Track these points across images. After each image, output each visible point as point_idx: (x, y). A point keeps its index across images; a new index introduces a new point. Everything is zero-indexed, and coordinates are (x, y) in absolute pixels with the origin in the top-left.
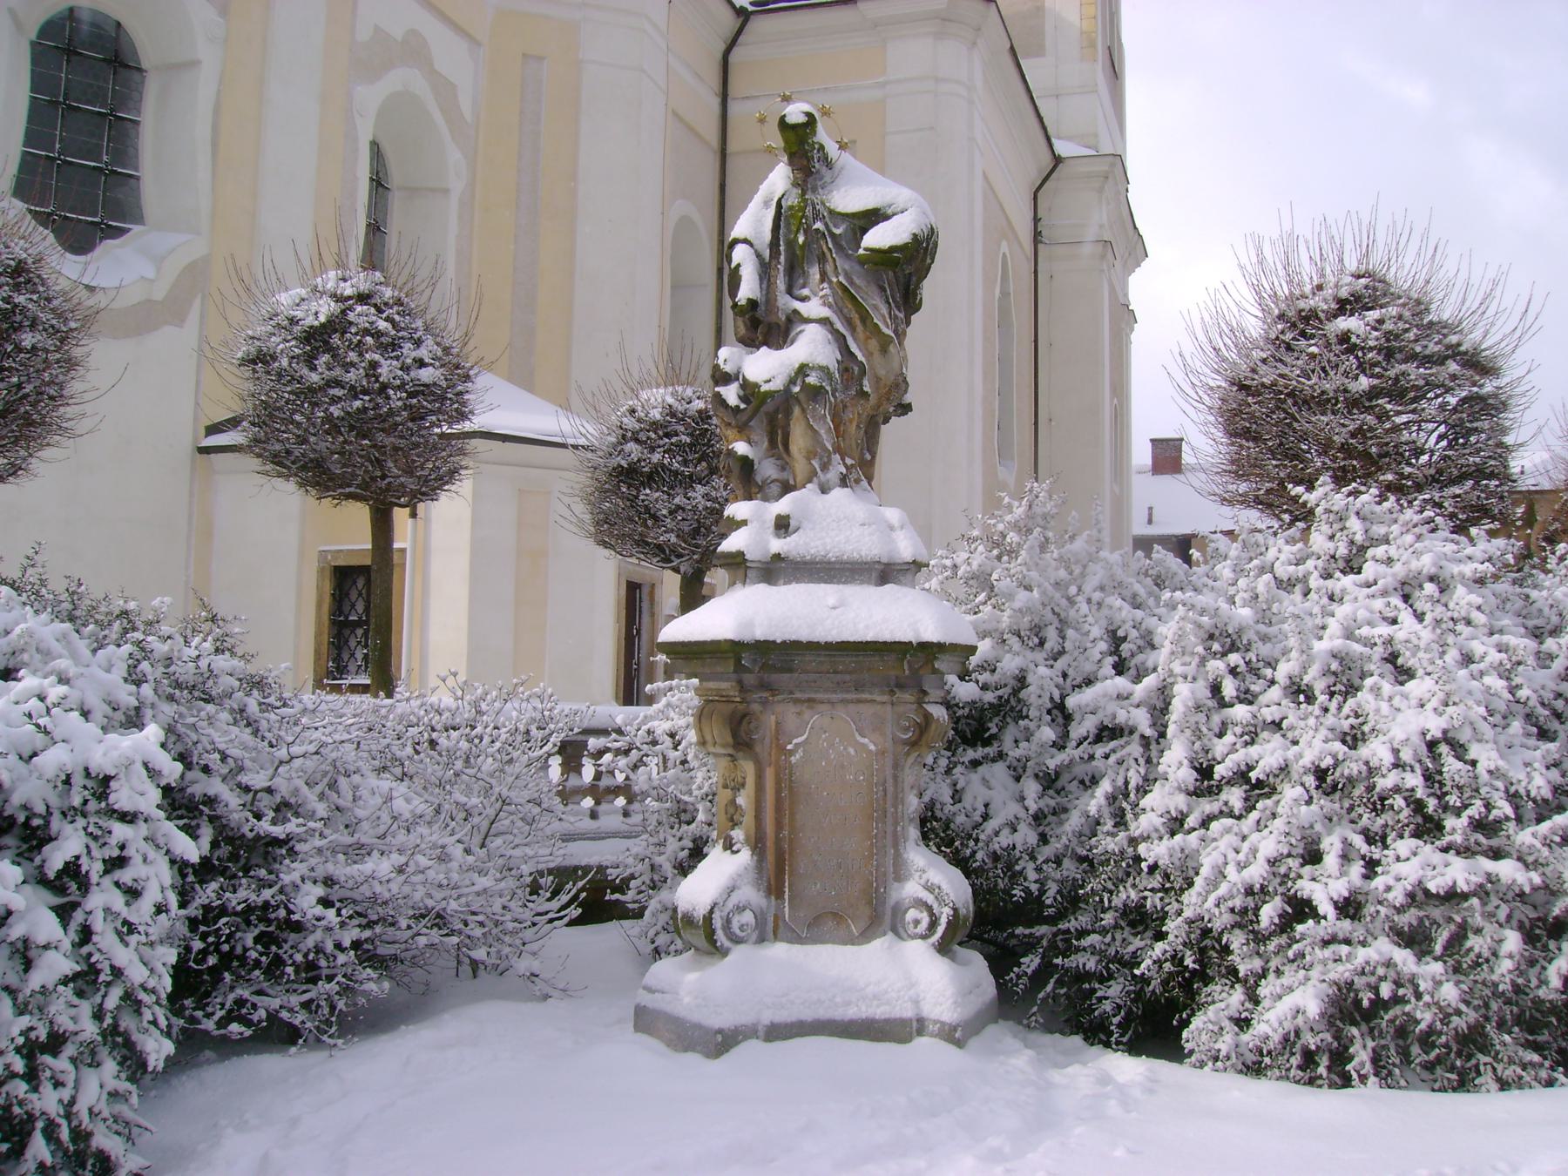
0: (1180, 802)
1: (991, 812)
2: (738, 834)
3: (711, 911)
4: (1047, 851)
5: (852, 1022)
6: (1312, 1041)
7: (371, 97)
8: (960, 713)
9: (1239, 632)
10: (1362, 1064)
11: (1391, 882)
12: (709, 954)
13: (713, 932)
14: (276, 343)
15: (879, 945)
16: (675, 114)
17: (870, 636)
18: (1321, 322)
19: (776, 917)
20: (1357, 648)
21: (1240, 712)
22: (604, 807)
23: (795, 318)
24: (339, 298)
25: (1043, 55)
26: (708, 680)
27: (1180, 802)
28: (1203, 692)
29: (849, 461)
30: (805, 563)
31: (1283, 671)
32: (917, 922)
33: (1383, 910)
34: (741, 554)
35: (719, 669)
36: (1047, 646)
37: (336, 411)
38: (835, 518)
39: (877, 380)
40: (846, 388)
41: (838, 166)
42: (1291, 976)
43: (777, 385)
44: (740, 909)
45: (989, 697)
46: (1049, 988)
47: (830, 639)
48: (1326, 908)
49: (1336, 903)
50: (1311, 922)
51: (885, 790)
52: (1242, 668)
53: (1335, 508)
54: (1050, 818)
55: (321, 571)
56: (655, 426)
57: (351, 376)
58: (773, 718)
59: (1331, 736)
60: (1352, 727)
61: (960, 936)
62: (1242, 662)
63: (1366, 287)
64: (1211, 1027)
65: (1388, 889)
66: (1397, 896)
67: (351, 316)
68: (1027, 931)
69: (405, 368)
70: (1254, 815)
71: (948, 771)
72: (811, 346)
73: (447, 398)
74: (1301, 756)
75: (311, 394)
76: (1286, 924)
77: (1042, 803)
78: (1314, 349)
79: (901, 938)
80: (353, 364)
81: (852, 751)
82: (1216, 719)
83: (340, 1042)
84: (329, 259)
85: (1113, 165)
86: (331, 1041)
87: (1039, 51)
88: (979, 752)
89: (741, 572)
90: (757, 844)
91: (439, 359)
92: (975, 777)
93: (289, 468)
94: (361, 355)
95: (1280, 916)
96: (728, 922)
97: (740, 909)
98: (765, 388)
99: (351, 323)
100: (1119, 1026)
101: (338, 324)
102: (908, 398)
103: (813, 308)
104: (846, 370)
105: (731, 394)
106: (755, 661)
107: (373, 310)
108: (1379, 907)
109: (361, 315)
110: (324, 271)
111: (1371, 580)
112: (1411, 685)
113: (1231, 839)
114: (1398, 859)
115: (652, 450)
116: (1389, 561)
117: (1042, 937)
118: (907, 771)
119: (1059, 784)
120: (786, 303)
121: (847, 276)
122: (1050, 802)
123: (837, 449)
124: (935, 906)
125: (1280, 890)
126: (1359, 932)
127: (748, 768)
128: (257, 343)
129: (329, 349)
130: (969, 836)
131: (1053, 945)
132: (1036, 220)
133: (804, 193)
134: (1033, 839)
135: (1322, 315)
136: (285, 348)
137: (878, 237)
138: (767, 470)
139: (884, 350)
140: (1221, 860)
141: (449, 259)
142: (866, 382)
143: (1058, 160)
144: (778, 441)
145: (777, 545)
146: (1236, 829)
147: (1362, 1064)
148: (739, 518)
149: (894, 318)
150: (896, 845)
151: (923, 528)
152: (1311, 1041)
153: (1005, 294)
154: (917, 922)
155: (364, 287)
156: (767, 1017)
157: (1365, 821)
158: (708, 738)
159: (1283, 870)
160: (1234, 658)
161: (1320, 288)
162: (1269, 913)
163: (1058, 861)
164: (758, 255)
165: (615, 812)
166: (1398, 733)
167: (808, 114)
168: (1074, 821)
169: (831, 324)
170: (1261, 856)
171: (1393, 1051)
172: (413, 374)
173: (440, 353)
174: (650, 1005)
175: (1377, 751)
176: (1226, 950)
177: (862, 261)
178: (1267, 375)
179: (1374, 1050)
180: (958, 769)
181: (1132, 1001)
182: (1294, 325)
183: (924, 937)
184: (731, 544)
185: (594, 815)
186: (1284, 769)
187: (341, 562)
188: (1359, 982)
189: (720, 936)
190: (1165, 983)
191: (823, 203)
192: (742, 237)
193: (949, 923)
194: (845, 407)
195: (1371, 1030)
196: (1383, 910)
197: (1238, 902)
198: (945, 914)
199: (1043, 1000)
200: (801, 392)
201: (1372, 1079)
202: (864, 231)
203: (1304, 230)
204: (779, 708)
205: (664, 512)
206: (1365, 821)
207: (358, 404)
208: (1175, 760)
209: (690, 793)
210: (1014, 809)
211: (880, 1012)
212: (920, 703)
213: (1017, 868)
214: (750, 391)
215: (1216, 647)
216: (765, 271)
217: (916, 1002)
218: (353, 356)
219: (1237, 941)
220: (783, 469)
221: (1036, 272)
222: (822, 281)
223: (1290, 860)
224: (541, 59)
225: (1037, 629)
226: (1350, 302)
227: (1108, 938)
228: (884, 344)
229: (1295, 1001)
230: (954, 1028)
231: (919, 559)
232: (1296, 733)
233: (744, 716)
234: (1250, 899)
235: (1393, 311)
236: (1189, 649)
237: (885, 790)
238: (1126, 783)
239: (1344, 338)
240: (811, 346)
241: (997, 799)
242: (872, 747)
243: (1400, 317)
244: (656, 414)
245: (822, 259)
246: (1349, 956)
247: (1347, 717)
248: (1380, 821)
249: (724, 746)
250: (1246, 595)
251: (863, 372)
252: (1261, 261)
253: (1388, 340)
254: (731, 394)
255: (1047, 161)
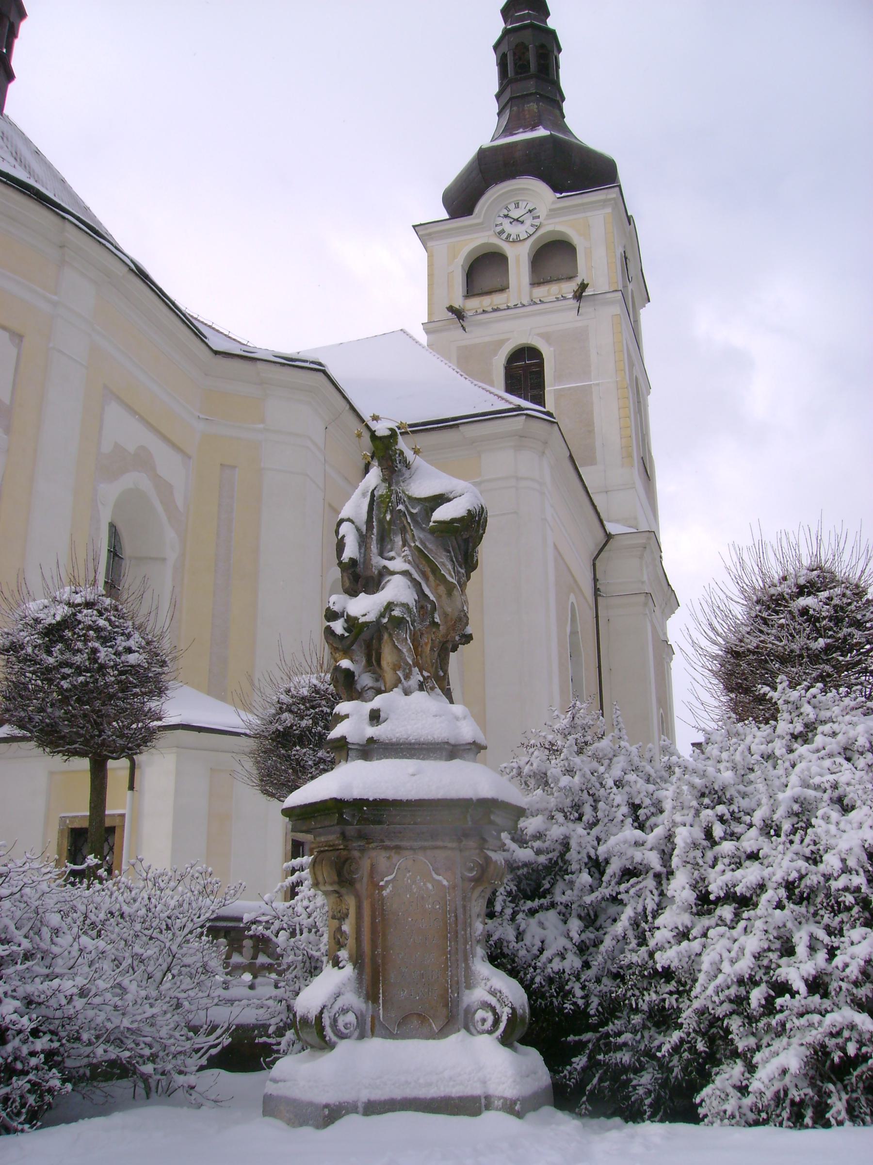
0: (686, 919)
1: (546, 946)
2: (343, 954)
3: (321, 1012)
4: (591, 973)
5: (433, 1100)
6: (796, 1094)
7: (110, 492)
8: (520, 872)
9: (724, 789)
10: (839, 1112)
11: (848, 960)
12: (322, 1049)
13: (322, 1029)
14: (25, 636)
15: (456, 1040)
16: (330, 505)
17: (440, 794)
18: (787, 602)
19: (373, 1017)
20: (811, 793)
21: (727, 847)
22: (260, 980)
23: (385, 572)
24: (69, 604)
25: (596, 464)
26: (320, 835)
27: (686, 919)
28: (699, 835)
29: (426, 674)
30: (392, 744)
31: (757, 818)
32: (484, 1020)
33: (844, 985)
34: (343, 738)
35: (327, 823)
36: (584, 818)
37: (65, 684)
38: (413, 712)
39: (445, 615)
40: (423, 621)
41: (414, 466)
42: (778, 1044)
43: (371, 617)
44: (344, 1011)
45: (542, 859)
46: (595, 1081)
47: (410, 798)
48: (799, 985)
49: (806, 981)
50: (787, 996)
51: (456, 916)
52: (727, 816)
53: (791, 699)
54: (592, 949)
55: (61, 832)
56: (303, 699)
57: (78, 659)
58: (369, 861)
59: (795, 857)
60: (812, 852)
61: (520, 1031)
62: (726, 812)
63: (818, 577)
64: (718, 1093)
65: (846, 965)
66: (853, 971)
67: (79, 617)
68: (577, 1038)
69: (118, 654)
70: (742, 924)
71: (513, 919)
72: (397, 590)
73: (148, 680)
74: (774, 874)
75: (47, 673)
76: (769, 1008)
77: (584, 936)
78: (783, 621)
79: (472, 1034)
80: (79, 651)
81: (430, 886)
82: (710, 855)
83: (26, 1126)
84: (65, 579)
85: (649, 538)
86: (20, 1127)
87: (592, 461)
88: (536, 903)
89: (344, 754)
90: (357, 960)
91: (144, 648)
92: (533, 921)
93: (31, 731)
94: (85, 644)
95: (766, 999)
96: (335, 1020)
97: (344, 1011)
98: (362, 620)
99: (80, 622)
100: (650, 1106)
101: (67, 623)
102: (469, 630)
103: (397, 564)
104: (422, 607)
105: (338, 627)
106: (354, 815)
107: (95, 612)
108: (841, 983)
109: (87, 616)
110: (63, 587)
111: (820, 746)
112: (853, 814)
113: (724, 942)
114: (852, 944)
115: (302, 718)
116: (834, 734)
117: (589, 1041)
118: (474, 903)
119: (598, 923)
120: (378, 561)
121: (422, 542)
122: (590, 935)
123: (416, 664)
124: (498, 1007)
125: (765, 978)
126: (827, 1003)
127: (351, 902)
128: (11, 637)
129: (62, 639)
130: (530, 965)
131: (597, 1049)
132: (595, 580)
133: (390, 485)
134: (578, 963)
135: (787, 596)
136: (30, 639)
137: (443, 513)
138: (365, 680)
139: (450, 593)
140: (717, 958)
141: (165, 602)
142: (436, 615)
143: (609, 537)
144: (373, 661)
145: (371, 731)
146: (728, 935)
147: (839, 1112)
148: (343, 713)
149: (457, 573)
150: (466, 960)
151: (481, 719)
152: (795, 1095)
153: (574, 633)
154: (484, 1020)
155: (90, 597)
156: (365, 1095)
157: (826, 920)
158: (320, 879)
159: (765, 962)
160: (721, 809)
161: (785, 579)
162: (757, 995)
163: (598, 981)
164: (358, 530)
165: (268, 984)
166: (843, 845)
167: (391, 430)
168: (608, 943)
169: (410, 575)
170: (748, 952)
171: (863, 1102)
172: (123, 658)
173: (144, 643)
174: (275, 1093)
175: (831, 862)
176: (727, 1031)
177: (432, 531)
178: (752, 642)
179: (848, 1101)
180: (520, 916)
181: (660, 1085)
182: (768, 608)
183: (490, 1032)
184: (336, 733)
185: (252, 987)
186: (762, 887)
187: (76, 825)
188: (831, 1043)
189: (328, 1032)
190: (684, 1069)
191: (403, 492)
192: (346, 517)
193: (509, 1020)
194: (422, 634)
195: (845, 1087)
196: (844, 985)
197: (733, 991)
198: (505, 1013)
199: (592, 1092)
200: (389, 622)
201: (847, 1123)
202: (433, 510)
203: (771, 538)
204: (373, 854)
205: (310, 763)
206: (826, 920)
207: (81, 679)
208: (680, 887)
209: (319, 950)
210: (563, 942)
211: (456, 1091)
212: (481, 849)
213: (567, 988)
214: (352, 623)
215: (706, 801)
216: (363, 540)
217: (484, 1082)
218: (80, 645)
219: (735, 1024)
220: (377, 680)
221: (597, 617)
222: (404, 546)
223: (770, 954)
224: (234, 467)
225: (577, 807)
226: (807, 587)
227: (638, 1037)
228: (450, 588)
229: (782, 1061)
230: (514, 1102)
231: (478, 741)
232: (770, 859)
233: (347, 860)
234: (742, 989)
235: (838, 591)
236: (686, 804)
237: (456, 916)
238: (645, 909)
239: (804, 611)
240: (397, 590)
241: (549, 936)
242: (445, 883)
243: (844, 595)
244: (305, 692)
245: (403, 531)
246: (820, 1023)
247: (809, 845)
248: (838, 919)
249: (331, 884)
250: (728, 765)
251: (434, 608)
252: (741, 561)
253: (836, 612)
254: (338, 627)
255: (601, 537)
